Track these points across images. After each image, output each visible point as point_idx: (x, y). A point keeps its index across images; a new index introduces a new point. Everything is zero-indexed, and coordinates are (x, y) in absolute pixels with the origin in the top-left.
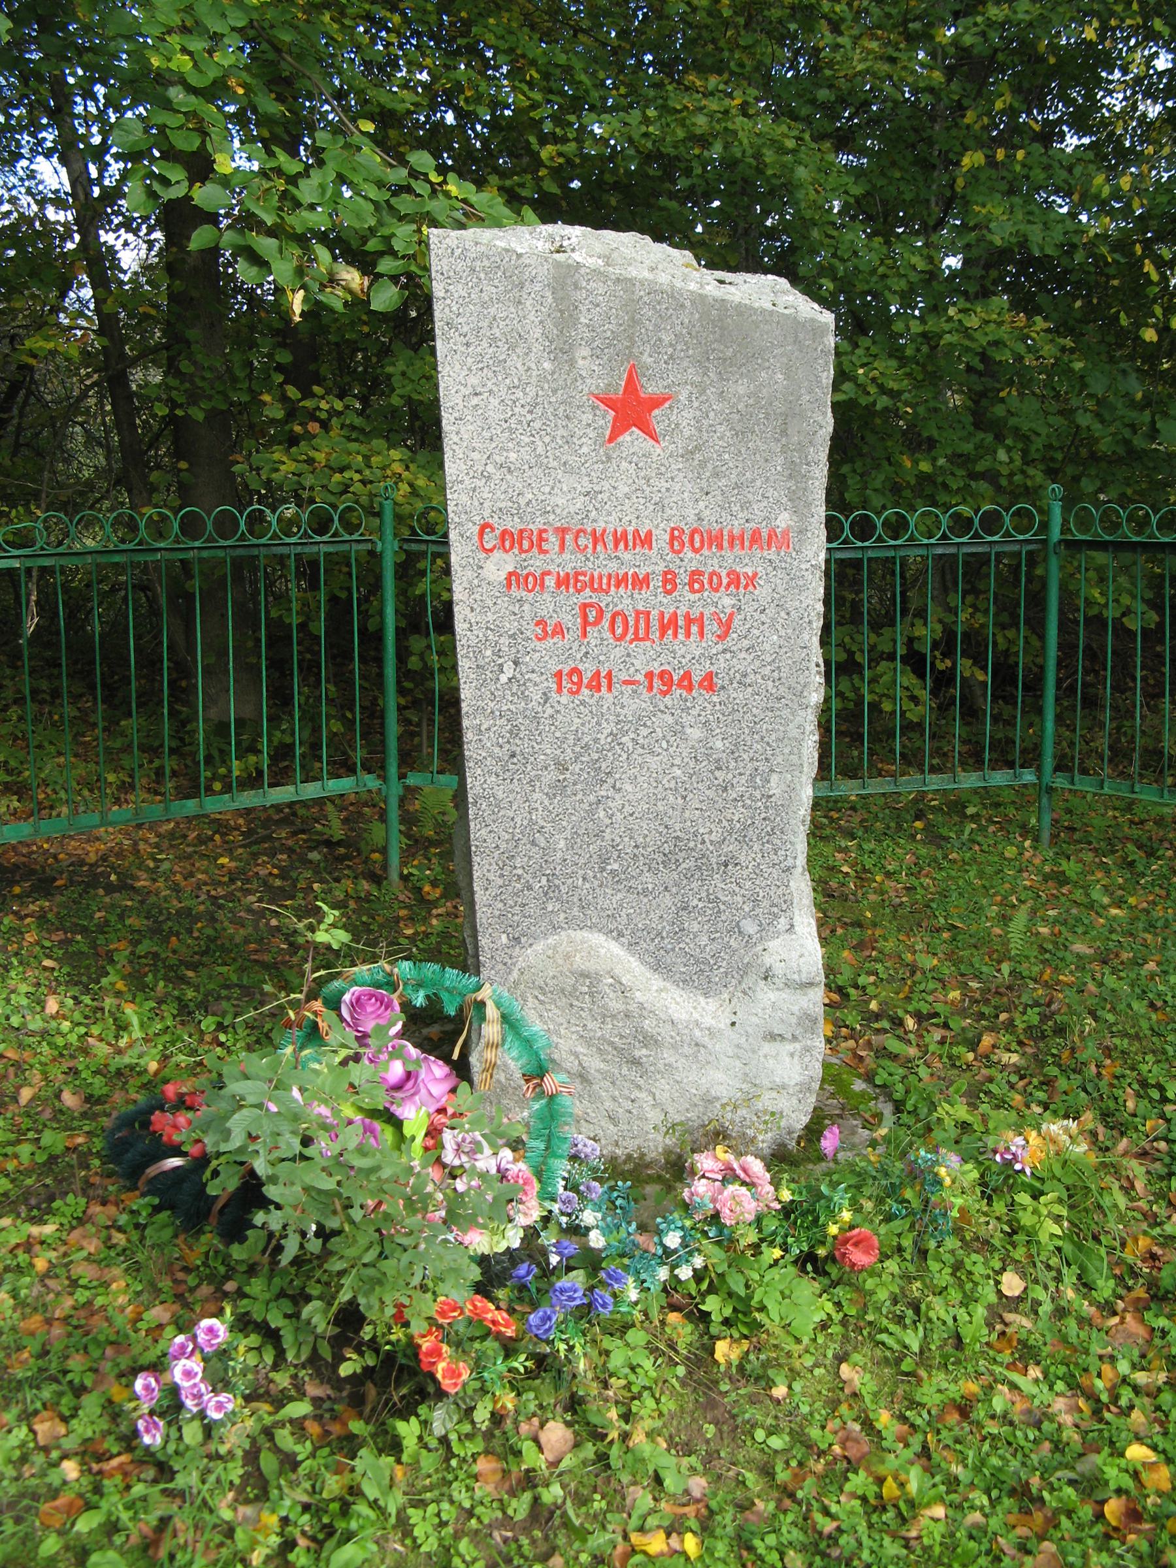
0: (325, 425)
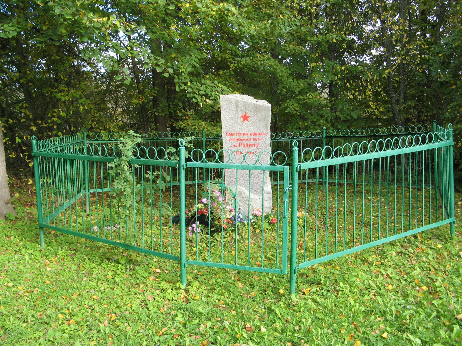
0: (189, 117)
